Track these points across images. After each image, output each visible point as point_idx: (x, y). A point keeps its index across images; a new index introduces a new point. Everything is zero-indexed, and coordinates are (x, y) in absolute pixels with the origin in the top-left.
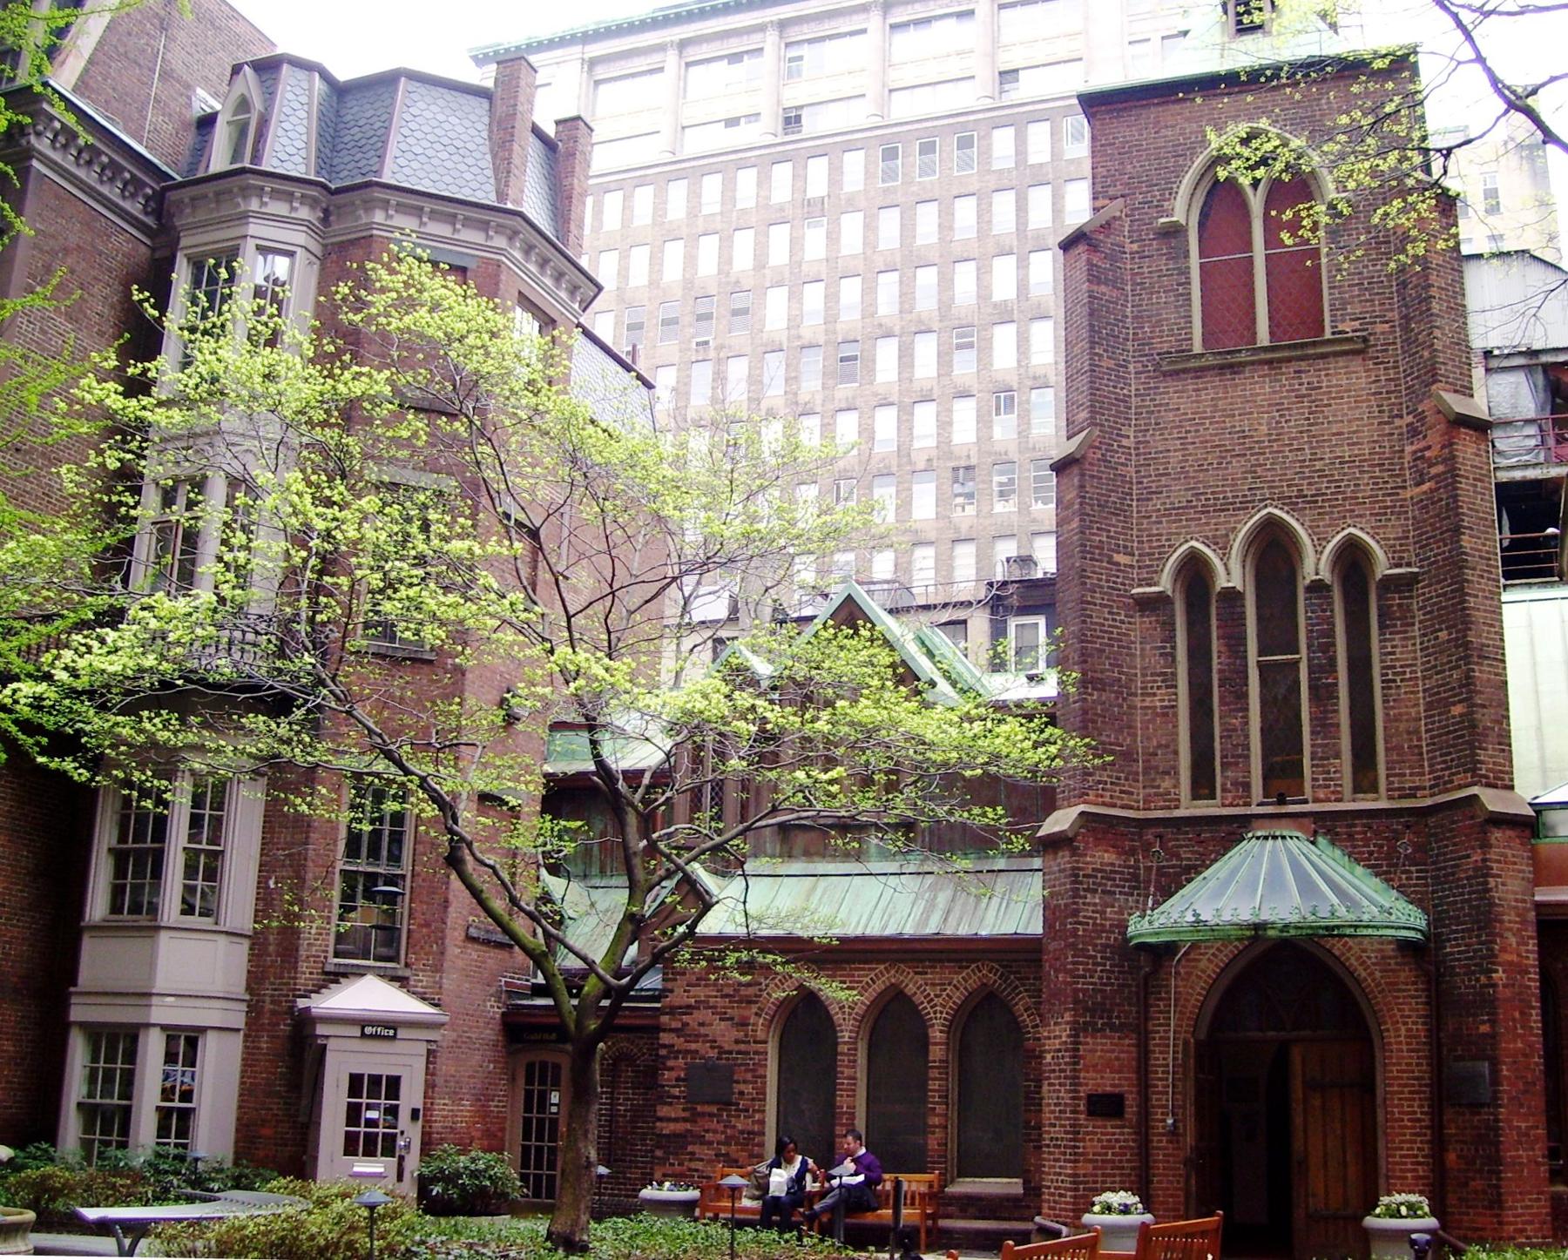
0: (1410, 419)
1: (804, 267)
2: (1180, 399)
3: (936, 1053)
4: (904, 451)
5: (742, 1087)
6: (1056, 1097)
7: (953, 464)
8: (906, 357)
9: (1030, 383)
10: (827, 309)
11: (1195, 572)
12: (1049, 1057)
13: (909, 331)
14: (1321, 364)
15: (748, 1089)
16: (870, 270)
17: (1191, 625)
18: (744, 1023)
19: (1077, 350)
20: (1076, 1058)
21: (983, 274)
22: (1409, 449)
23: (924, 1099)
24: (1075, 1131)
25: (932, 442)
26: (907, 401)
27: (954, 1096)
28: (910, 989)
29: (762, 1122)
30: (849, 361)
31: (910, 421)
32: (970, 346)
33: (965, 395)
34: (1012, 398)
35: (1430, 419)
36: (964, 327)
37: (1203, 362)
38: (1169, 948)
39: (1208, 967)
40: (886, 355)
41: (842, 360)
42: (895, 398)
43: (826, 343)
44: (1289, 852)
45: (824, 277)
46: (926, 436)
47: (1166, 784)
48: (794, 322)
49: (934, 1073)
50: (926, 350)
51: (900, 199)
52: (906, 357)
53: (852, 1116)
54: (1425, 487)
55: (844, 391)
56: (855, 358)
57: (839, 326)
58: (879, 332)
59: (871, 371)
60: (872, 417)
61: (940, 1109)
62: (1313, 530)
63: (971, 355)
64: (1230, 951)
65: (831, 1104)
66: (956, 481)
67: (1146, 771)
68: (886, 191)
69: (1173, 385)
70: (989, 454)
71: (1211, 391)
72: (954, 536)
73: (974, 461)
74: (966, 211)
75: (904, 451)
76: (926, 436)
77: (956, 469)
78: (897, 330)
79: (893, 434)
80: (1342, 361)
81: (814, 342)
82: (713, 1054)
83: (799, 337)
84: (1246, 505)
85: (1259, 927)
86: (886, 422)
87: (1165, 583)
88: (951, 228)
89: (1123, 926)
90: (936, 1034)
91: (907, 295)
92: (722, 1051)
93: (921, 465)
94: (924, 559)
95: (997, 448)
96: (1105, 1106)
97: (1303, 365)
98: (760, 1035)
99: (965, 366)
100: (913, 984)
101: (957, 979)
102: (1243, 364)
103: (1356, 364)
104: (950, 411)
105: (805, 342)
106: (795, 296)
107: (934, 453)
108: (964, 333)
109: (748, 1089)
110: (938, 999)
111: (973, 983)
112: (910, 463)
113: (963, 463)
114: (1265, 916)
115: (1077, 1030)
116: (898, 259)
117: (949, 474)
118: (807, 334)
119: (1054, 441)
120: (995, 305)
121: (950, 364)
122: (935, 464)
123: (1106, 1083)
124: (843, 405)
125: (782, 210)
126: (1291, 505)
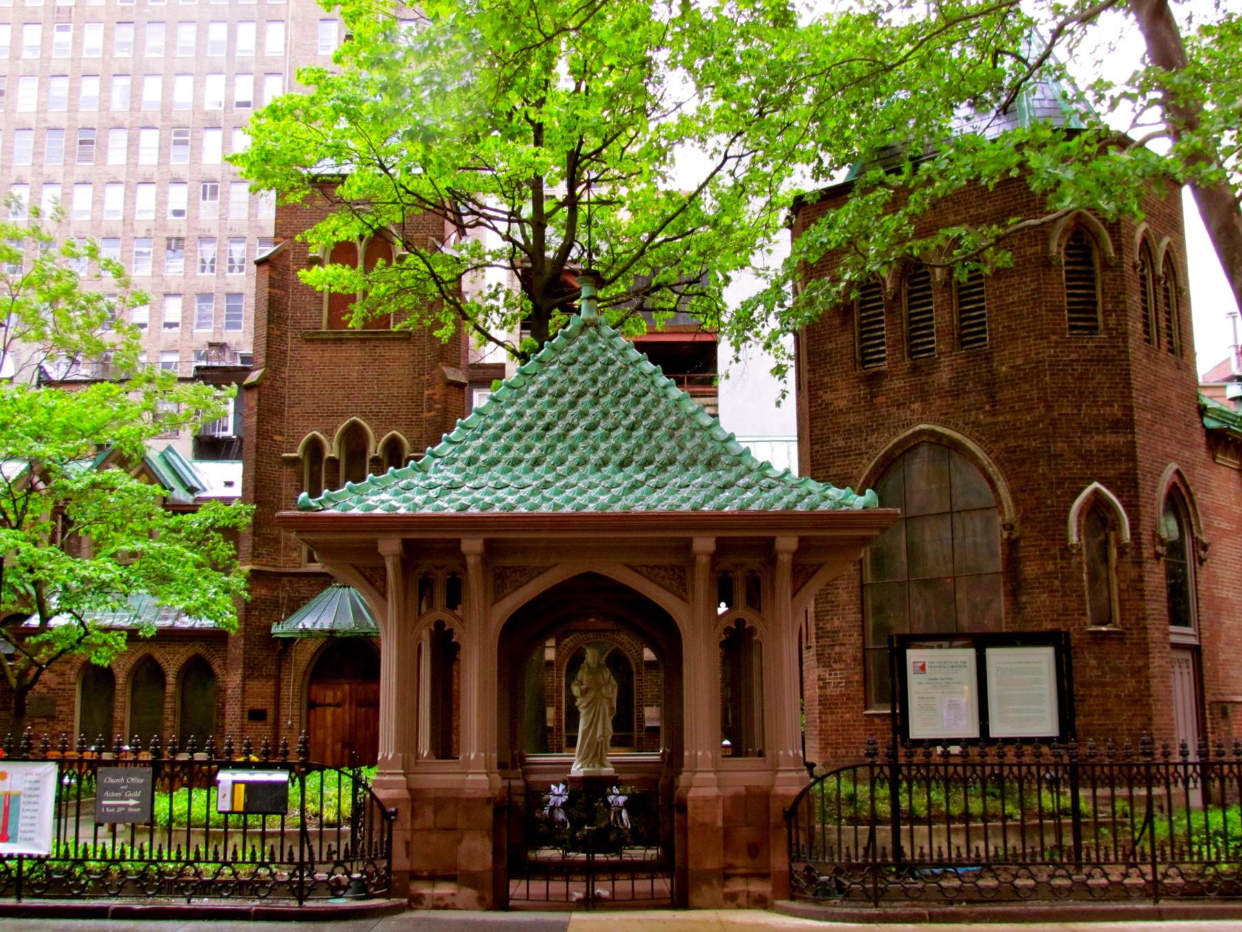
0: (427, 377)
1: (53, 63)
2: (313, 355)
3: (170, 689)
4: (128, 221)
5: (61, 708)
6: (233, 711)
7: (167, 235)
8: (133, 145)
9: (231, 178)
10: (70, 100)
11: (315, 448)
12: (229, 692)
13: (136, 127)
14: (386, 343)
15: (65, 709)
16: (107, 74)
17: (311, 475)
18: (63, 674)
19: (260, 324)
20: (244, 691)
21: (199, 85)
22: (426, 393)
23: (161, 713)
24: (242, 728)
25: (151, 216)
26: (134, 180)
27: (178, 710)
28: (157, 656)
29: (72, 727)
30: (88, 142)
31: (134, 197)
32: (185, 143)
33: (178, 181)
34: (216, 187)
35: (437, 380)
36: (181, 130)
37: (326, 336)
38: (292, 640)
39: (312, 647)
40: (117, 142)
41: (81, 142)
42: (122, 178)
43: (69, 127)
44: (350, 594)
45: (68, 73)
46: (147, 211)
47: (295, 555)
48: (42, 109)
49: (167, 699)
50: (150, 139)
51: (134, 18)
52: (133, 145)
53: (123, 723)
54: (432, 413)
55: (82, 168)
56: (92, 142)
57: (79, 116)
58: (113, 124)
59: (104, 153)
60: (103, 191)
61: (171, 718)
62: (376, 430)
63: (186, 150)
64: (320, 642)
65: (111, 716)
66: (169, 248)
67: (285, 548)
68: (123, 9)
69: (311, 347)
70: (197, 229)
71: (329, 352)
72: (165, 291)
73: (183, 235)
74: (187, 35)
75: (128, 221)
76: (147, 211)
77: (169, 239)
78: (127, 124)
79: (120, 207)
80: (397, 343)
81: (58, 126)
82: (45, 690)
83: (46, 121)
84: (343, 415)
85: (331, 632)
86: (114, 197)
87: (298, 453)
88: (174, 47)
89: (269, 628)
90: (171, 679)
91: (135, 94)
92: (50, 689)
93: (142, 233)
94: (90, 87)
95: (202, 226)
96: (257, 715)
97: (377, 343)
98: (72, 680)
99: (179, 160)
100: (159, 654)
101: (182, 650)
102: (348, 339)
103: (404, 345)
104: (166, 193)
105: (52, 125)
106: (43, 86)
107: (153, 226)
108: (181, 135)
109: (65, 709)
110: (172, 662)
111: (191, 653)
112: (133, 230)
113: (175, 235)
114: (336, 627)
115: (245, 678)
116: (131, 67)
117: (165, 242)
118: (53, 120)
119: (246, 224)
120: (207, 113)
121: (168, 156)
122: (153, 233)
123: (258, 704)
124: (81, 180)
125: (35, 12)
126: (364, 415)
